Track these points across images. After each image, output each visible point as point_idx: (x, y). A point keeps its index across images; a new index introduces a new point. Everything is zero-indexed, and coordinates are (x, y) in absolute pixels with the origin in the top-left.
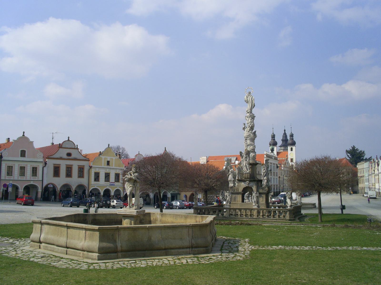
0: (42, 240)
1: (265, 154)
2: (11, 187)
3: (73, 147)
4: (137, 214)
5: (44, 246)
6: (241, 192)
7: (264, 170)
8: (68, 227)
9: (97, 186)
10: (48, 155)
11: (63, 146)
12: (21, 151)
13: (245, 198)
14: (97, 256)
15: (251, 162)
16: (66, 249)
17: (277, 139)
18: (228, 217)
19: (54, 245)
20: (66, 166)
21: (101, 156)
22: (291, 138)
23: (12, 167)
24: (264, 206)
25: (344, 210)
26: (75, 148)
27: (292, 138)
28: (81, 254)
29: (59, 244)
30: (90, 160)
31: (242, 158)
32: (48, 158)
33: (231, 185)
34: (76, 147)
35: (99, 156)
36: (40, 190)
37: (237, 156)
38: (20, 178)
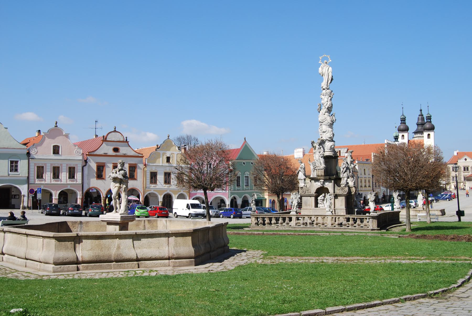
0: (4, 252)
1: (386, 144)
2: (41, 193)
3: (122, 140)
4: (122, 220)
5: (6, 258)
6: (314, 193)
7: (344, 164)
8: (27, 235)
9: (170, 191)
10: (89, 151)
11: (108, 139)
12: (54, 146)
13: (319, 201)
14: (52, 268)
15: (327, 154)
16: (25, 260)
17: (408, 123)
18: (295, 227)
19: (14, 256)
20: (97, 165)
21: (159, 151)
22: (402, 122)
23: (43, 167)
24: (344, 212)
25: (462, 218)
26: (124, 141)
27: (430, 121)
28: (39, 266)
29: (20, 256)
30: (144, 156)
31: (315, 149)
32: (89, 155)
33: (301, 184)
34: (125, 139)
35: (156, 150)
36: (79, 196)
37: (348, 146)
38: (53, 182)
